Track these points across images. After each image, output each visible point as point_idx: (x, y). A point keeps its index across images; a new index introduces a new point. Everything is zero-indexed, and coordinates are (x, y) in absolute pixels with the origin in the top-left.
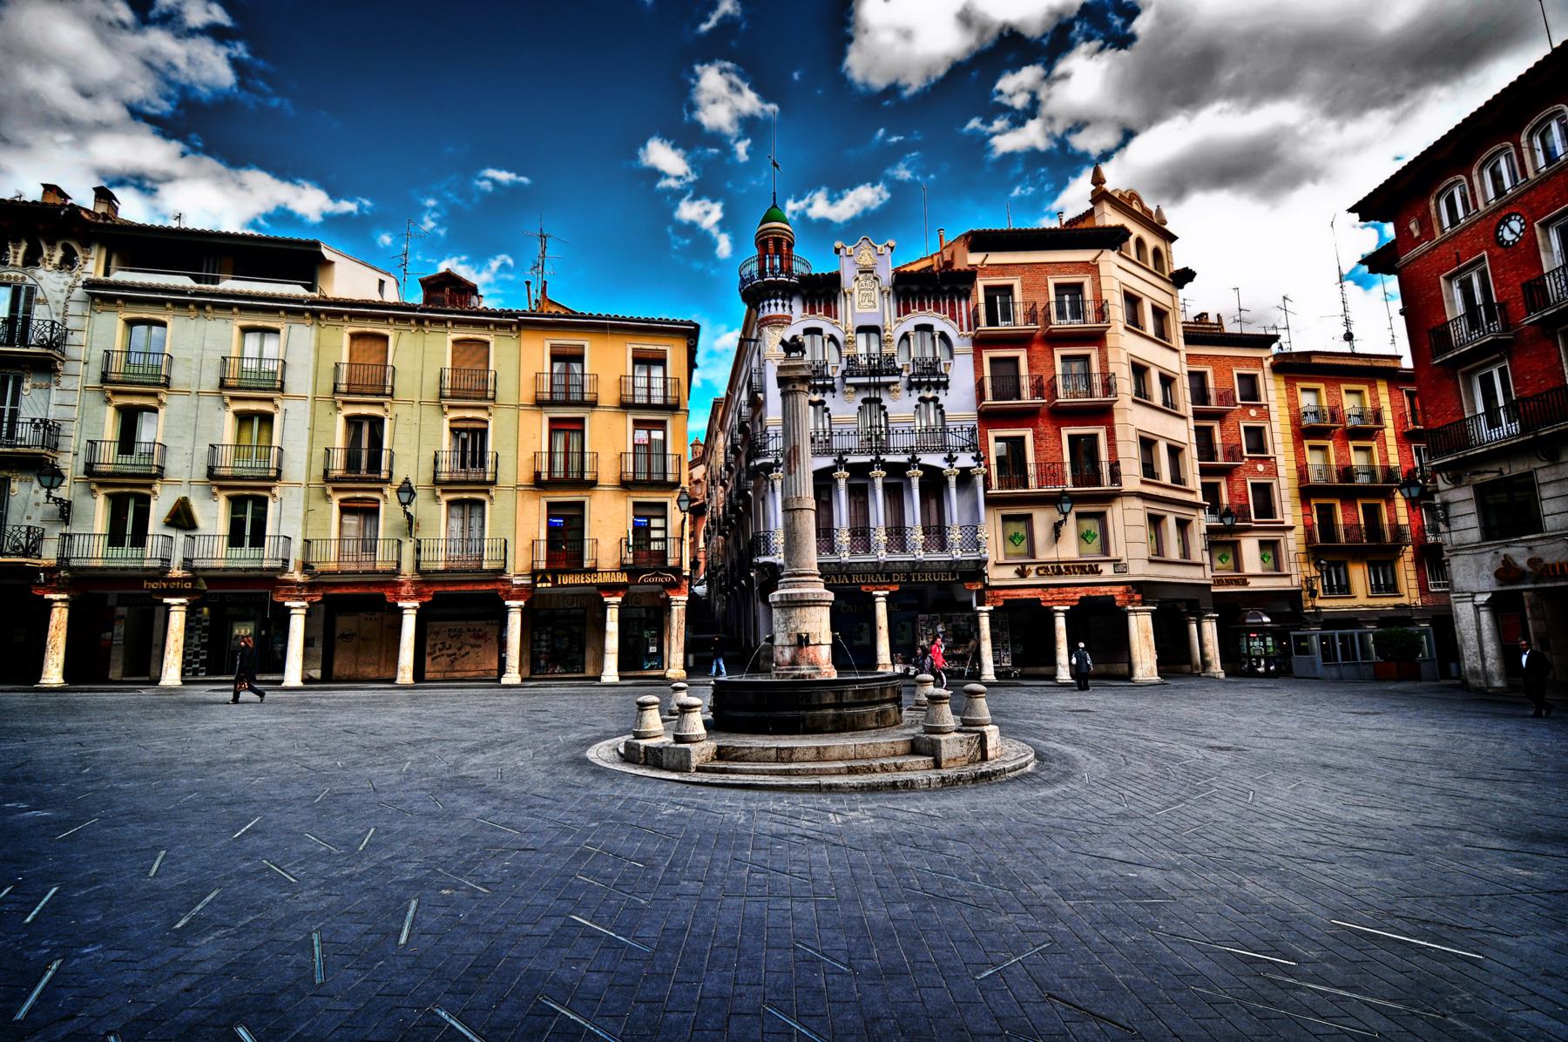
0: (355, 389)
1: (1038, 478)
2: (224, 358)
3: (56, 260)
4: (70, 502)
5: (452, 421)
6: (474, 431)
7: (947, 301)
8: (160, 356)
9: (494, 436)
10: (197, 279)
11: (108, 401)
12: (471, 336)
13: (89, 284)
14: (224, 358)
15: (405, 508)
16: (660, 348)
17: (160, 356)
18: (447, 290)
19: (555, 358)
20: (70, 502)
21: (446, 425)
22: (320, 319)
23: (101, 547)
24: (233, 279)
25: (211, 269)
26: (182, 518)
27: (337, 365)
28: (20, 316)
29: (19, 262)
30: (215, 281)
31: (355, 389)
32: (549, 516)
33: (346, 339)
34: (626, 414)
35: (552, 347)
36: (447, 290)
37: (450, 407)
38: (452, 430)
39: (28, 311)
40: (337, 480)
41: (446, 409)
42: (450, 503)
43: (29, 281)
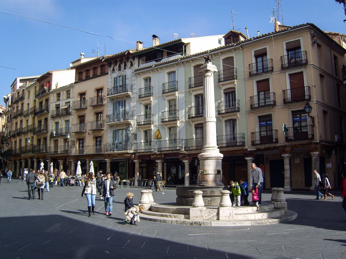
0: (291, 66)
1: (226, 103)
2: (249, 65)
3: (129, 66)
4: (314, 117)
5: (224, 90)
6: (232, 92)
7: (161, 54)
8: (252, 64)
9: (238, 93)
10: (156, 61)
11: (141, 103)
12: (227, 56)
13: (136, 70)
14: (249, 65)
15: (309, 114)
16: (297, 39)
17: (252, 64)
18: (232, 37)
19: (256, 57)
20: (314, 117)
21: (222, 91)
22: (185, 64)
23: (257, 138)
24: (146, 63)
25: (161, 57)
26: (158, 138)
27: (190, 78)
28: (124, 84)
29: (123, 69)
30: (160, 60)
31: (291, 66)
32: (260, 122)
33: (192, 69)
34: (285, 72)
35: (255, 52)
36: (232, 37)
37: (222, 85)
38: (224, 93)
39: (125, 82)
40: (193, 117)
41: (221, 86)
42: (226, 121)
43: (125, 74)
